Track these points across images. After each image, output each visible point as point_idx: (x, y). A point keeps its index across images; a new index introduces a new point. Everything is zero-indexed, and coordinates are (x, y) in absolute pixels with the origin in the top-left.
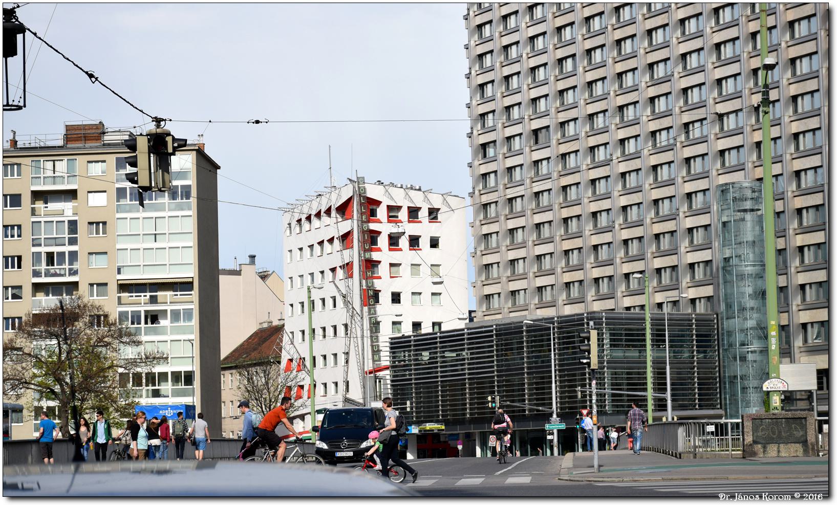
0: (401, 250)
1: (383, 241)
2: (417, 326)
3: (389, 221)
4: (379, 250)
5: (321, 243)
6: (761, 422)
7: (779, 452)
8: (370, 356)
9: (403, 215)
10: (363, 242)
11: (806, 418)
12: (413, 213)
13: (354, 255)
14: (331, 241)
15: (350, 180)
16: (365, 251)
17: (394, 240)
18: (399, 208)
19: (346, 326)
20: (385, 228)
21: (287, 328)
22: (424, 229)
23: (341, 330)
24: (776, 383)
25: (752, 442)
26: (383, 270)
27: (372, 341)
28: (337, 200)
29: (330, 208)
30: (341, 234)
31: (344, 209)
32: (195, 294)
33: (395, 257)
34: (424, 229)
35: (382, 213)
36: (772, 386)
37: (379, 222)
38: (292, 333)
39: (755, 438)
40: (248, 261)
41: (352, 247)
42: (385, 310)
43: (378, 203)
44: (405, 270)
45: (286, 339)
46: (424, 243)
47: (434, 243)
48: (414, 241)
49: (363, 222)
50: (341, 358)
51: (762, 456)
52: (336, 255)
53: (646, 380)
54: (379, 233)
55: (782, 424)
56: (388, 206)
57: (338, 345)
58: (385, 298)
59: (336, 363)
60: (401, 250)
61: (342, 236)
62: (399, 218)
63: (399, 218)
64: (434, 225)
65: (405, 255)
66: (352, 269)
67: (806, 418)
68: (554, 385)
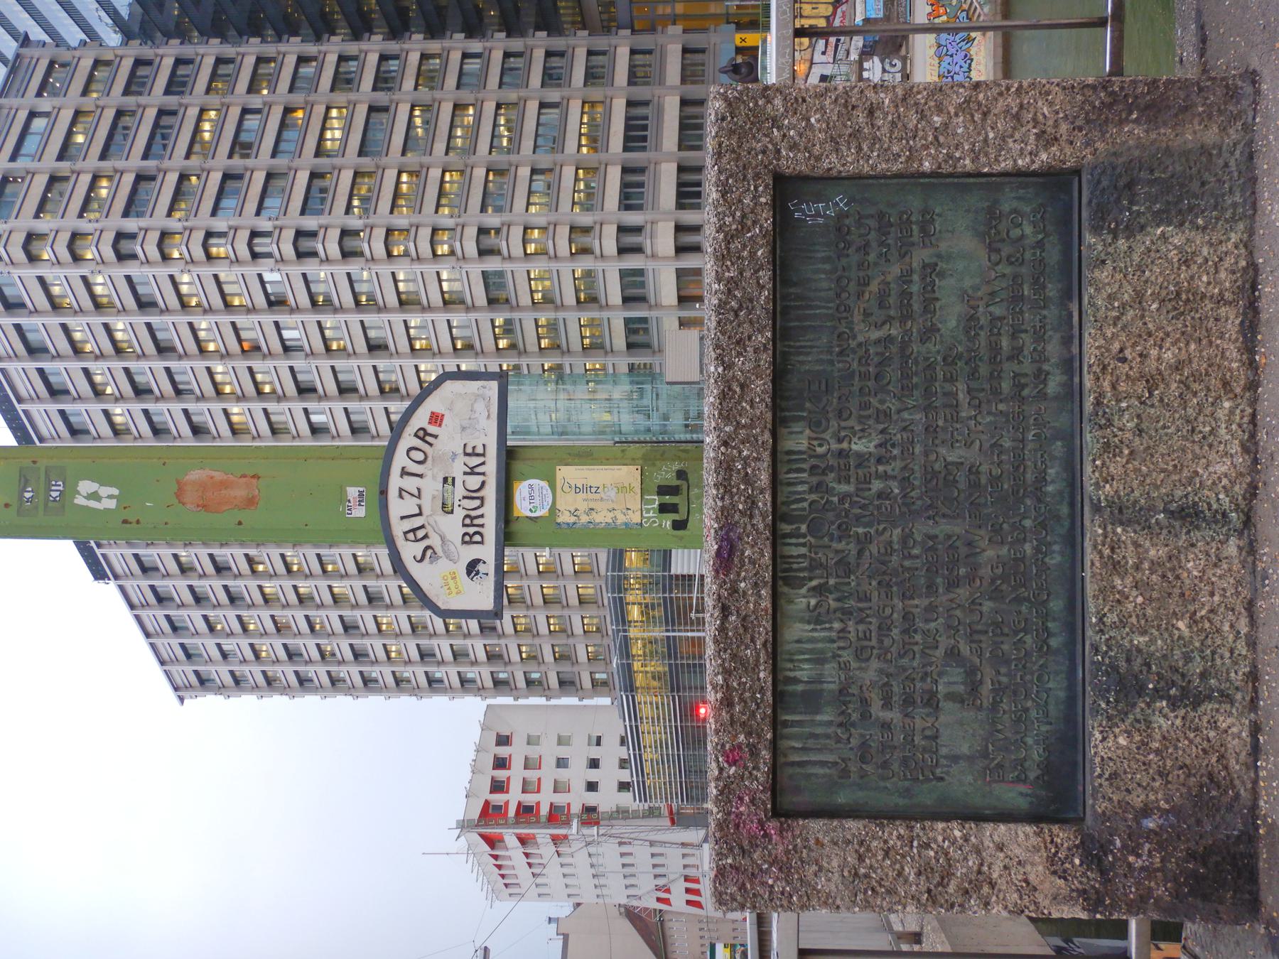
4: (538, 804)
5: (530, 865)
6: (812, 700)
7: (1188, 515)
8: (655, 819)
10: (528, 824)
11: (780, 181)
12: (501, 763)
13: (543, 835)
14: (527, 855)
15: (458, 837)
16: (538, 822)
19: (620, 844)
20: (514, 797)
21: (624, 901)
22: (516, 753)
23: (625, 849)
24: (431, 486)
25: (1064, 836)
27: (638, 817)
29: (492, 856)
30: (519, 844)
31: (491, 841)
35: (498, 799)
36: (452, 526)
37: (507, 803)
38: (628, 897)
39: (1013, 795)
40: (554, 925)
41: (533, 835)
42: (608, 799)
43: (487, 803)
44: (563, 774)
45: (635, 903)
47: (531, 741)
49: (506, 824)
50: (656, 850)
51: (1234, 725)
52: (545, 849)
55: (845, 462)
56: (491, 792)
57: (642, 855)
58: (591, 799)
59: (661, 855)
64: (515, 740)
65: (548, 773)
66: (558, 835)
67: (780, 181)
68: (690, 634)
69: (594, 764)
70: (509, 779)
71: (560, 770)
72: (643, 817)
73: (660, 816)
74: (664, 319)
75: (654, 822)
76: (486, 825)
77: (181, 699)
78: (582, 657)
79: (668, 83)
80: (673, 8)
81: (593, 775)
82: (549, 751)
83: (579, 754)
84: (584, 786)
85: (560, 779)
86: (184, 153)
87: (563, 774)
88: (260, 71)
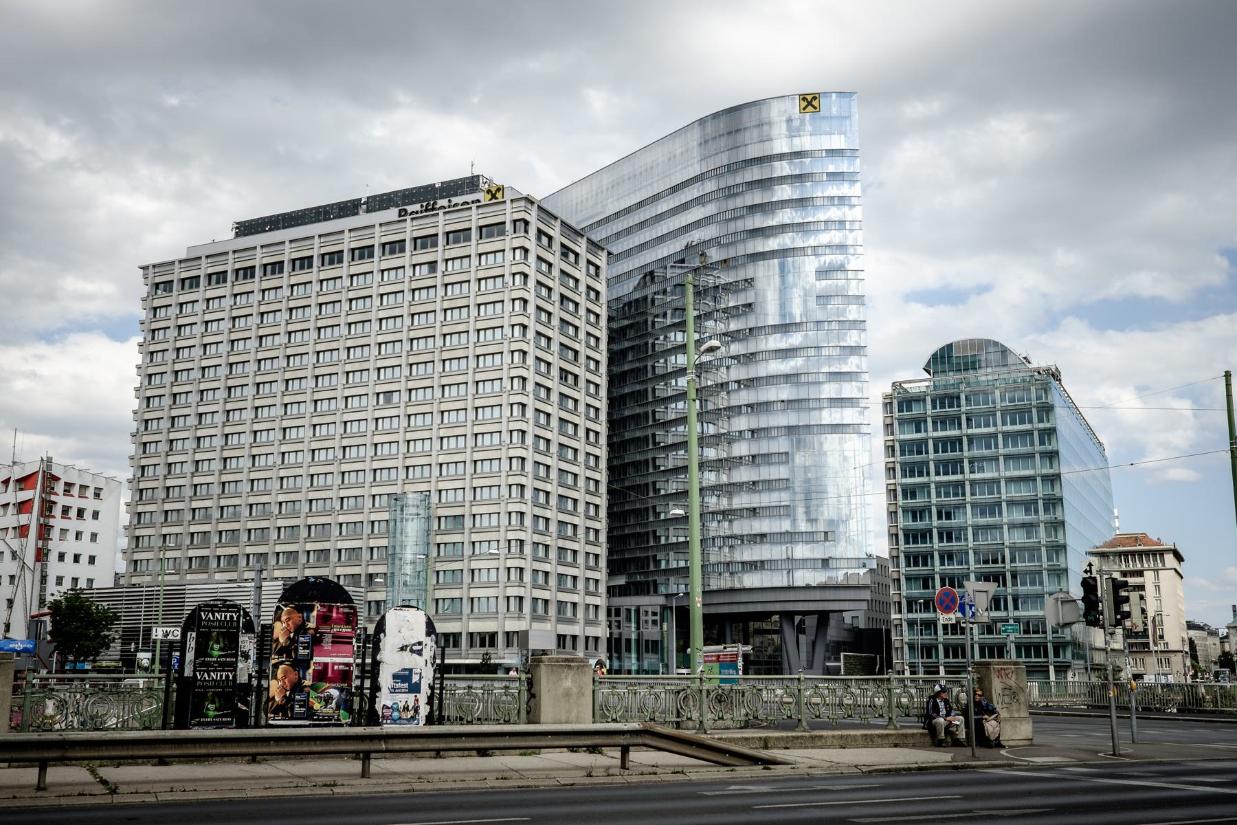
0: (70, 518)
1: (57, 511)
2: (90, 581)
3: (64, 495)
9: (90, 493)
13: (32, 519)
17: (66, 510)
18: (87, 487)
19: (12, 577)
22: (90, 504)
26: (55, 534)
28: (18, 473)
31: (25, 482)
32: (751, 629)
33: (64, 524)
34: (90, 504)
35: (60, 488)
44: (71, 536)
46: (88, 515)
48: (80, 513)
53: (918, 476)
54: (55, 503)
56: (65, 483)
60: (70, 518)
61: (20, 503)
62: (645, 655)
63: (645, 655)
65: (73, 524)
69: (76, 558)
70: (72, 496)
71: (89, 537)
72: (40, 595)
73: (40, 607)
74: (460, 623)
75: (36, 602)
76: (44, 477)
77: (143, 268)
78: (942, 670)
79: (558, 626)
80: (367, 689)
81: (84, 559)
82: (88, 525)
83: (85, 548)
84: (62, 550)
85: (68, 533)
86: (539, 356)
87: (71, 536)
88: (570, 352)
